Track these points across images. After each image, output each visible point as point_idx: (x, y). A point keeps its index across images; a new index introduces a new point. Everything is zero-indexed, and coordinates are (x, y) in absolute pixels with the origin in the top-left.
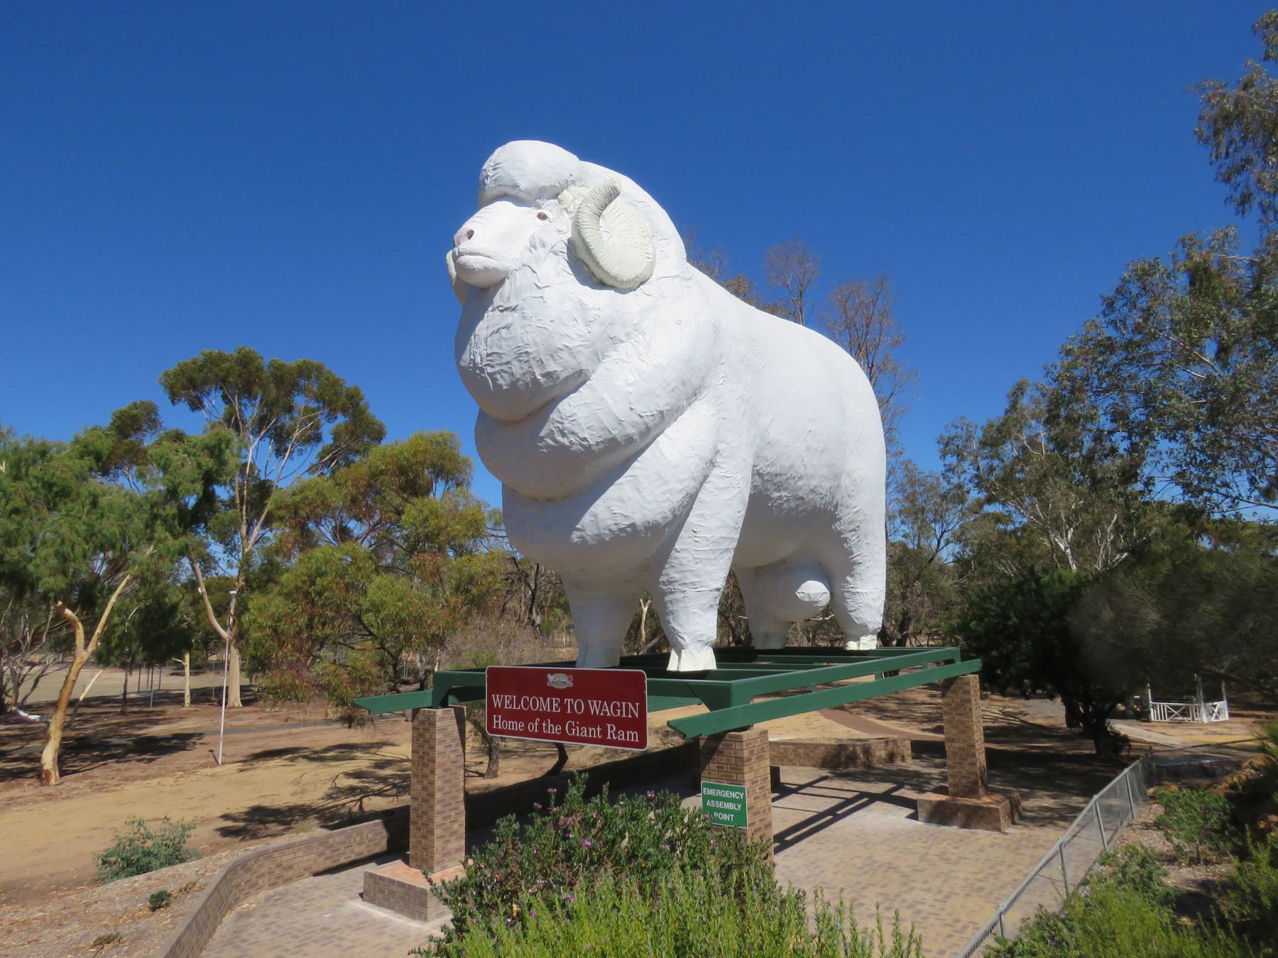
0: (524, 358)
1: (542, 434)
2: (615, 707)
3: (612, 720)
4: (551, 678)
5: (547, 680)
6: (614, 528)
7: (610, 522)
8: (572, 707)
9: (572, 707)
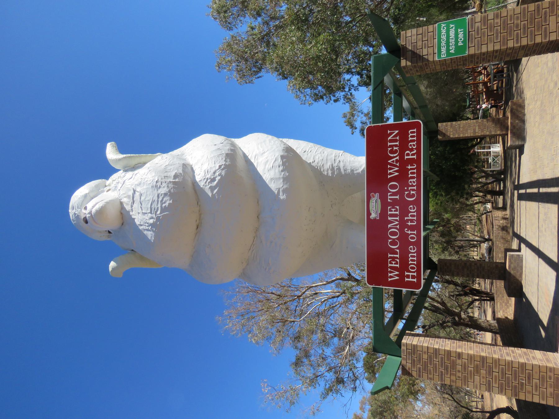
0: (159, 184)
1: (210, 195)
2: (392, 152)
3: (402, 155)
4: (373, 216)
5: (375, 219)
6: (281, 168)
7: (277, 170)
8: (394, 194)
9: (394, 194)
